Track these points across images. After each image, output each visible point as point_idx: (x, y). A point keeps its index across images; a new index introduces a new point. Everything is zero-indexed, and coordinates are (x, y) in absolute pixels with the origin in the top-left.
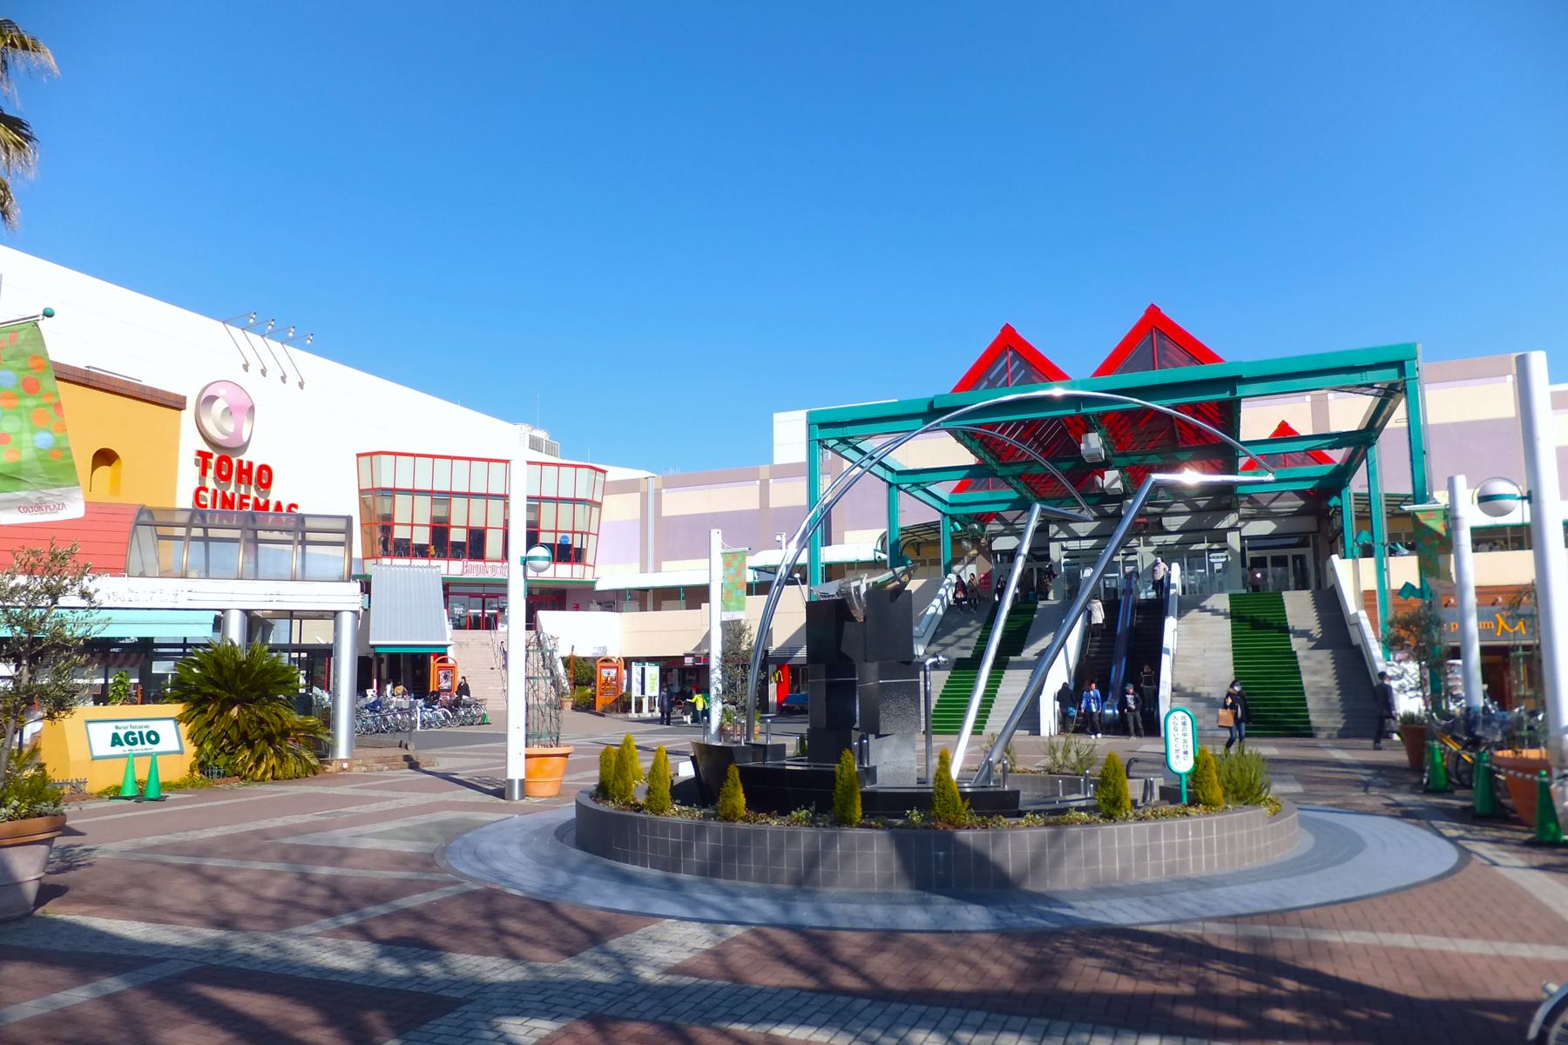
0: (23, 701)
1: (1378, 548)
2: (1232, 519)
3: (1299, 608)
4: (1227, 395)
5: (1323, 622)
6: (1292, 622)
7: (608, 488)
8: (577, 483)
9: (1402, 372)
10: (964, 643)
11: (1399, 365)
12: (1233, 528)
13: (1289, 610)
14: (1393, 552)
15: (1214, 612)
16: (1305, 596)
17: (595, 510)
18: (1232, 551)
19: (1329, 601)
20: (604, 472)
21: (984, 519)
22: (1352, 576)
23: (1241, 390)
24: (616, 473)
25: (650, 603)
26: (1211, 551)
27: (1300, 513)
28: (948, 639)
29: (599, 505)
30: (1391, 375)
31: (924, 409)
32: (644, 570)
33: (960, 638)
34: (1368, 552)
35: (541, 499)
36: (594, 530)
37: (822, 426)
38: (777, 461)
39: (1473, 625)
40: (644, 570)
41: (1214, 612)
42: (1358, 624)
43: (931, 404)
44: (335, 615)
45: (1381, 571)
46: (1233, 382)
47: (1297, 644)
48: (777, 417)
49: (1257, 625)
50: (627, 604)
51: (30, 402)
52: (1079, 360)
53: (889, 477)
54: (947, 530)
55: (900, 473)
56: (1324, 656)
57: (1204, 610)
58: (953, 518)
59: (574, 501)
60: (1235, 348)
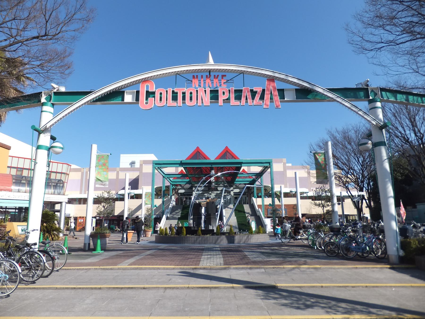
0: (4, 220)
1: (262, 196)
2: (232, 188)
3: (247, 208)
4: (240, 166)
5: (251, 211)
6: (246, 211)
7: (71, 170)
8: (63, 168)
9: (270, 164)
10: (178, 214)
11: (269, 163)
12: (232, 191)
13: (245, 208)
14: (265, 197)
15: (230, 208)
16: (248, 205)
17: (67, 176)
18: (232, 195)
19: (252, 207)
20: (71, 166)
21: (177, 185)
22: (257, 202)
23: (243, 165)
24: (73, 166)
25: (82, 202)
26: (227, 195)
27: (182, 175)
28: (174, 213)
29: (68, 175)
30: (268, 165)
31: (180, 162)
32: (81, 193)
33: (177, 213)
34: (260, 197)
35: (51, 172)
36: (66, 181)
37: (156, 164)
38: (121, 167)
39: (284, 212)
40: (81, 193)
41: (230, 208)
42: (259, 211)
43: (181, 161)
44: (61, 203)
45: (263, 201)
46: (241, 163)
47: (247, 215)
48: (121, 155)
49: (239, 211)
50: (74, 202)
51: (104, 167)
52: (212, 155)
53: (164, 175)
54: (171, 188)
55: (166, 174)
56: (253, 217)
57: (228, 208)
58: (173, 185)
59: (62, 173)
60: (242, 158)
